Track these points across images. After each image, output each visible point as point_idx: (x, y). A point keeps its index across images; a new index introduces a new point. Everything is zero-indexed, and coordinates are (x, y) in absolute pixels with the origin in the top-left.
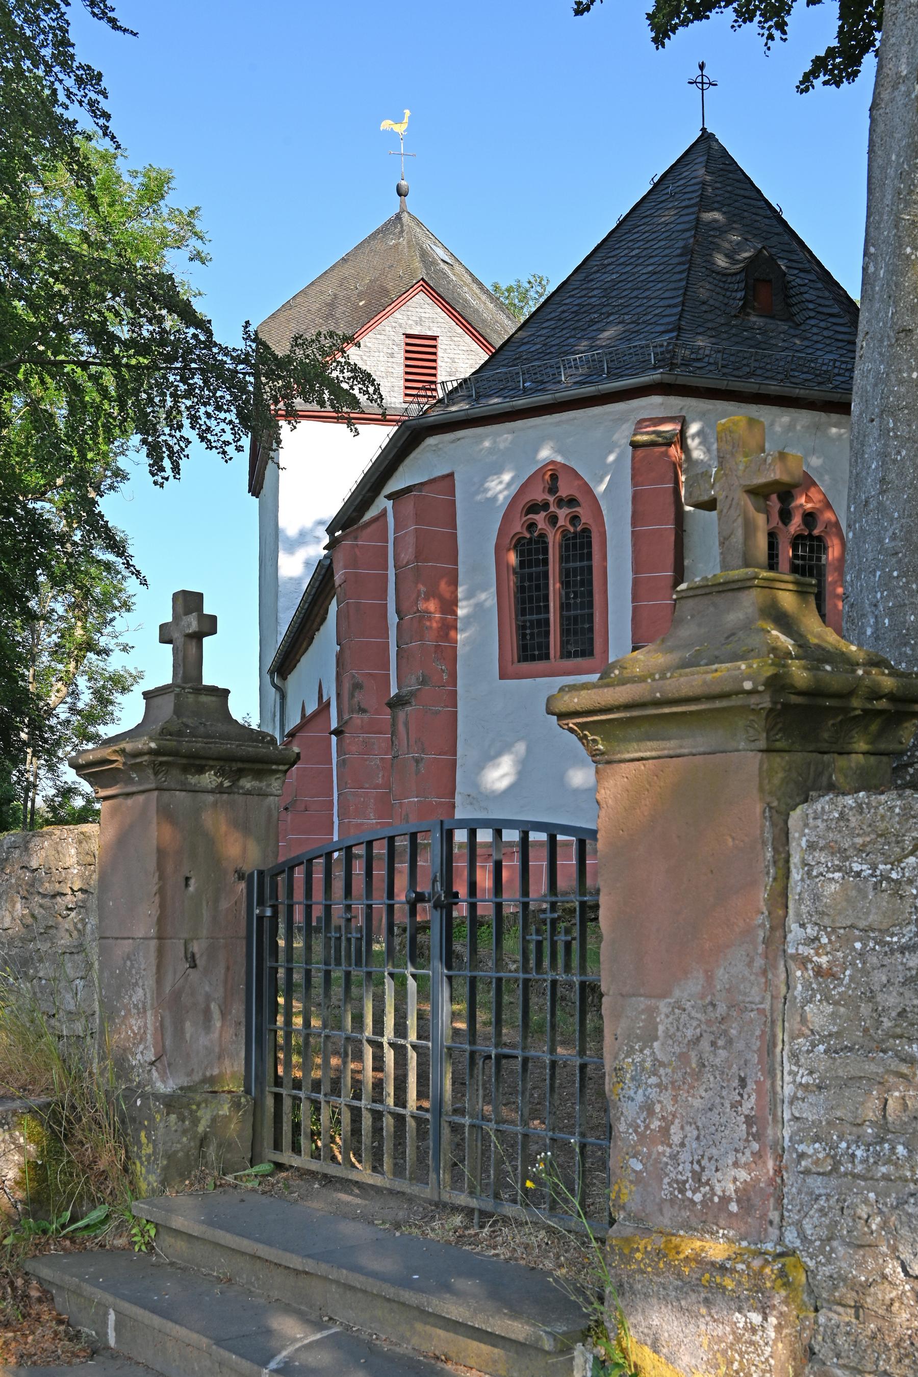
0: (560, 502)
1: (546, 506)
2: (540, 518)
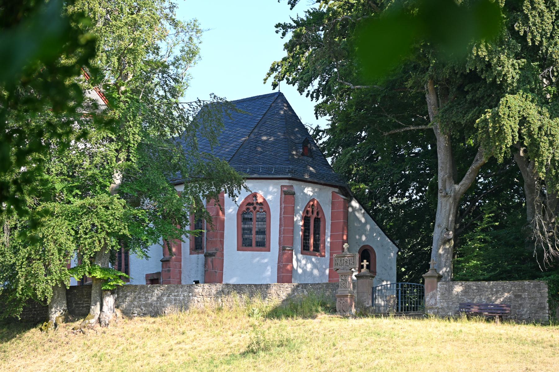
1: (253, 204)
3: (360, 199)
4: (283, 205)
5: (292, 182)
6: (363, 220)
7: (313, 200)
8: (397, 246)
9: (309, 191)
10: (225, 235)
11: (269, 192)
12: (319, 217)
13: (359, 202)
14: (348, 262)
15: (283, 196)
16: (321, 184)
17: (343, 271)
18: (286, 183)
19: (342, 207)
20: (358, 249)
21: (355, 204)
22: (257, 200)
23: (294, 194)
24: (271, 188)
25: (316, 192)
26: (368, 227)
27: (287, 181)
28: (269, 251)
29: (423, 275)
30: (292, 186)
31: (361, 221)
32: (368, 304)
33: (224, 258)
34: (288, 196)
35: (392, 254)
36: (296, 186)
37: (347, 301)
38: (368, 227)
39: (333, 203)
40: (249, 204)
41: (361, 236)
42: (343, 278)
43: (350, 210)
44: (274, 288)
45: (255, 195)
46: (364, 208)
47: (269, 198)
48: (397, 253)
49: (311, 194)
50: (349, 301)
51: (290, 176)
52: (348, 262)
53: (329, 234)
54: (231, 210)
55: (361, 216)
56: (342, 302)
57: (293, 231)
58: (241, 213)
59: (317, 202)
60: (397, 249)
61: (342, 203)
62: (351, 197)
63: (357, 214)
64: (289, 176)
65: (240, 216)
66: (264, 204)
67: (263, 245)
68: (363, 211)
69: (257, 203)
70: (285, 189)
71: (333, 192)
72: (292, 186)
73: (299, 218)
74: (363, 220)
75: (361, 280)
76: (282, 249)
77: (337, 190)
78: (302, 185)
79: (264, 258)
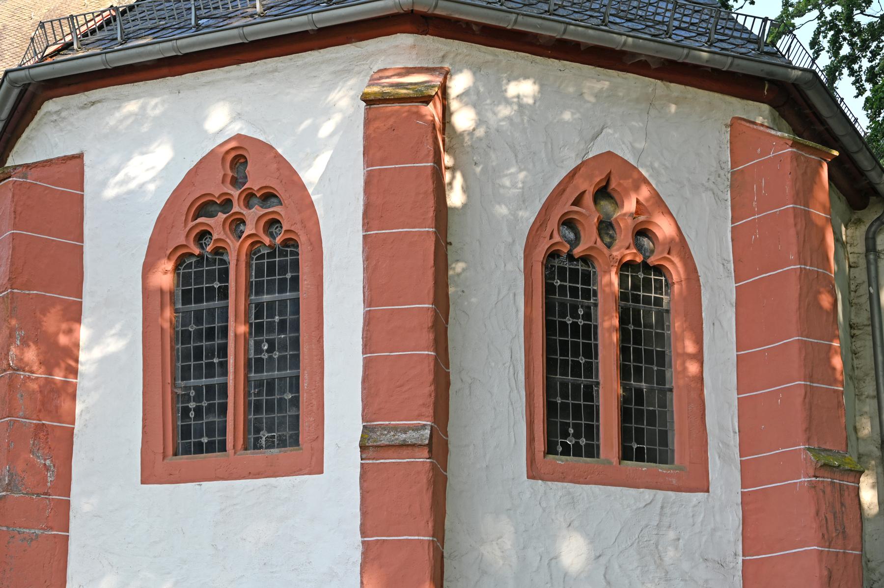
0: (249, 198)
2: (216, 223)
11: (314, 122)
27: (404, 40)
39: (739, 185)
71: (735, 124)
77: (760, 113)
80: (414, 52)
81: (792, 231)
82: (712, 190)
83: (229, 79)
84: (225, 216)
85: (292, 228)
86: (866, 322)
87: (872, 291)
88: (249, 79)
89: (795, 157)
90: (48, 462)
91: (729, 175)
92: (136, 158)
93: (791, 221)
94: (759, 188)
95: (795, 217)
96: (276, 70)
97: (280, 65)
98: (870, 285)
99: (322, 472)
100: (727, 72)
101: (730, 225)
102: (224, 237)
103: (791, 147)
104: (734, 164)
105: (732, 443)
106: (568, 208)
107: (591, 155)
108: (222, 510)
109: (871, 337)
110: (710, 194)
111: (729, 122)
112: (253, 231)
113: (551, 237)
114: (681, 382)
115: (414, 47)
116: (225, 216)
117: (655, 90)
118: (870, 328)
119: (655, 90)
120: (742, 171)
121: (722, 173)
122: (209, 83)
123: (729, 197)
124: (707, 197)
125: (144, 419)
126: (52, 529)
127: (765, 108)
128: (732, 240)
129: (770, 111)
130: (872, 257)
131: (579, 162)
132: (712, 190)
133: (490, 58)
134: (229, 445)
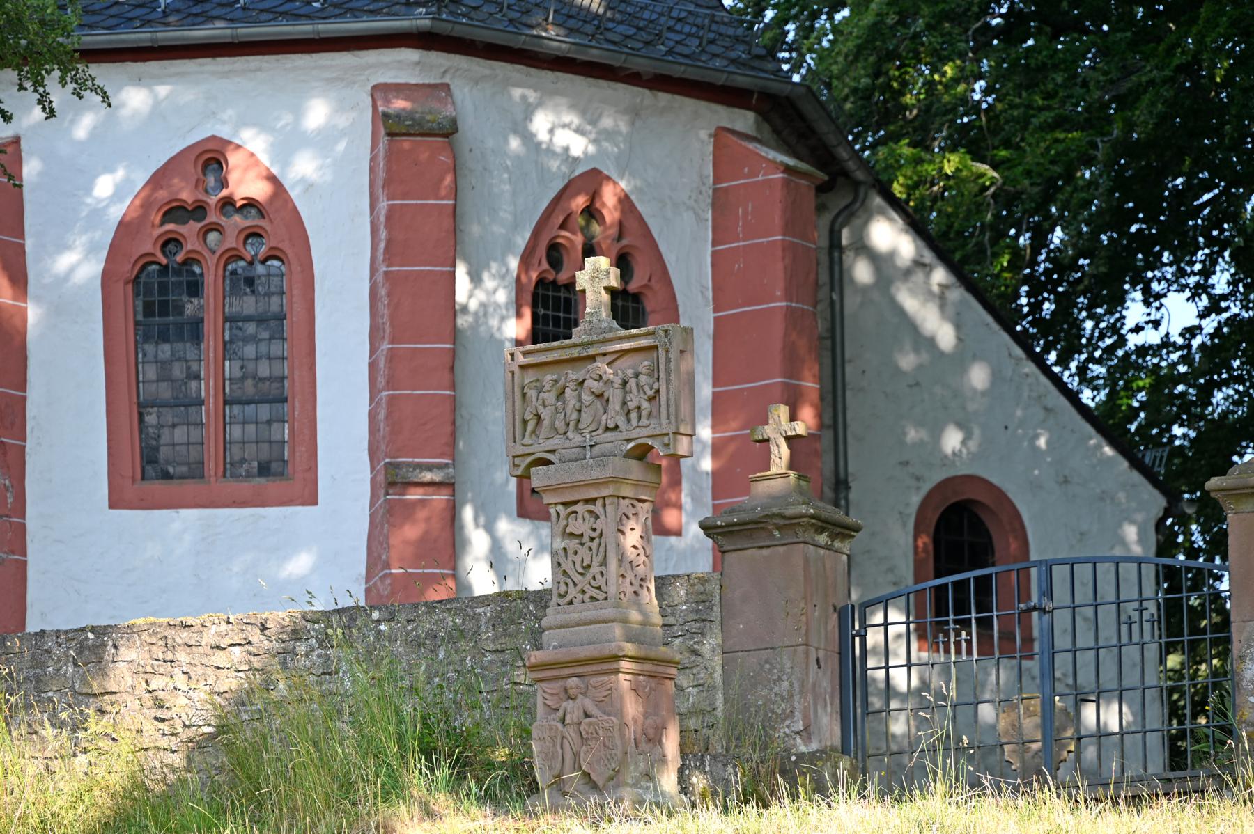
2: (189, 230)
3: (945, 235)
4: (383, 205)
5: (439, 59)
6: (946, 336)
7: (592, 180)
8: (1155, 483)
9: (562, 129)
10: (31, 410)
11: (302, 138)
12: (633, 287)
13: (916, 225)
14: (615, 395)
15: (383, 142)
16: (633, 78)
17: (577, 473)
18: (401, 66)
19: (777, 219)
20: (916, 500)
21: (888, 235)
22: (223, 183)
23: (449, 131)
24: (317, 113)
25: (609, 135)
26: (979, 376)
27: (410, 55)
28: (313, 501)
29: (1213, 483)
30: (446, 87)
31: (931, 342)
32: (806, 733)
33: (31, 558)
34: (415, 147)
35: (1131, 532)
36: (472, 89)
37: (610, 703)
38: (979, 376)
39: (720, 202)
40: (176, 212)
41: (937, 434)
42: (577, 526)
43: (862, 272)
44: (126, 653)
45: (211, 158)
46: (944, 257)
47: (303, 170)
48: (1160, 523)
49: (578, 146)
50: (632, 708)
51: (425, 23)
52: (615, 395)
53: (705, 391)
54: (65, 261)
55: (931, 309)
56: (572, 709)
57: (451, 363)
58: (127, 269)
59: (625, 202)
60: (1161, 502)
61: (778, 194)
62: (856, 184)
63: (909, 302)
64: (420, 19)
65: (124, 292)
66: (274, 217)
67: (276, 470)
68: (940, 275)
69: (228, 202)
70: (400, 104)
71: (720, 134)
72: (446, 87)
73: (502, 296)
74: (946, 336)
75: (746, 559)
76: (391, 481)
77: (744, 120)
78: (508, 83)
79: (285, 550)
80: (418, 68)
81: (780, 266)
82: (693, 209)
83: (202, 73)
84: (199, 225)
85: (280, 246)
86: (825, 335)
87: (835, 297)
88: (225, 75)
89: (786, 183)
90: (7, 482)
91: (711, 192)
92: (97, 151)
93: (779, 253)
94: (745, 213)
95: (784, 250)
96: (259, 69)
97: (265, 65)
98: (832, 289)
99: (315, 503)
100: (722, 86)
101: (709, 249)
102: (199, 249)
103: (783, 172)
104: (717, 179)
105: (705, 485)
106: (555, 232)
107: (577, 173)
108: (204, 539)
109: (829, 354)
110: (691, 213)
111: (713, 131)
112: (234, 245)
113: (539, 263)
114: (98, 234)
115: (418, 63)
116: (199, 225)
117: (642, 101)
118: (829, 343)
119: (642, 101)
120: (726, 189)
121: (704, 189)
122: (178, 74)
123: (709, 215)
124: (688, 217)
125: (109, 440)
126: (13, 553)
127: (750, 116)
128: (713, 265)
129: (757, 122)
130: (836, 254)
131: (566, 181)
132: (693, 209)
133: (487, 72)
134: (211, 467)
